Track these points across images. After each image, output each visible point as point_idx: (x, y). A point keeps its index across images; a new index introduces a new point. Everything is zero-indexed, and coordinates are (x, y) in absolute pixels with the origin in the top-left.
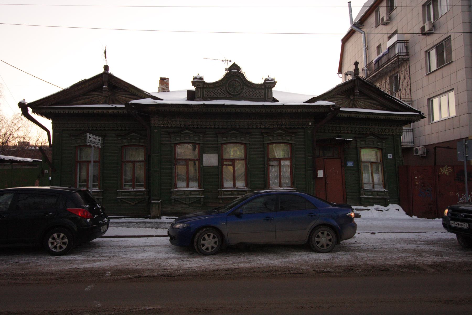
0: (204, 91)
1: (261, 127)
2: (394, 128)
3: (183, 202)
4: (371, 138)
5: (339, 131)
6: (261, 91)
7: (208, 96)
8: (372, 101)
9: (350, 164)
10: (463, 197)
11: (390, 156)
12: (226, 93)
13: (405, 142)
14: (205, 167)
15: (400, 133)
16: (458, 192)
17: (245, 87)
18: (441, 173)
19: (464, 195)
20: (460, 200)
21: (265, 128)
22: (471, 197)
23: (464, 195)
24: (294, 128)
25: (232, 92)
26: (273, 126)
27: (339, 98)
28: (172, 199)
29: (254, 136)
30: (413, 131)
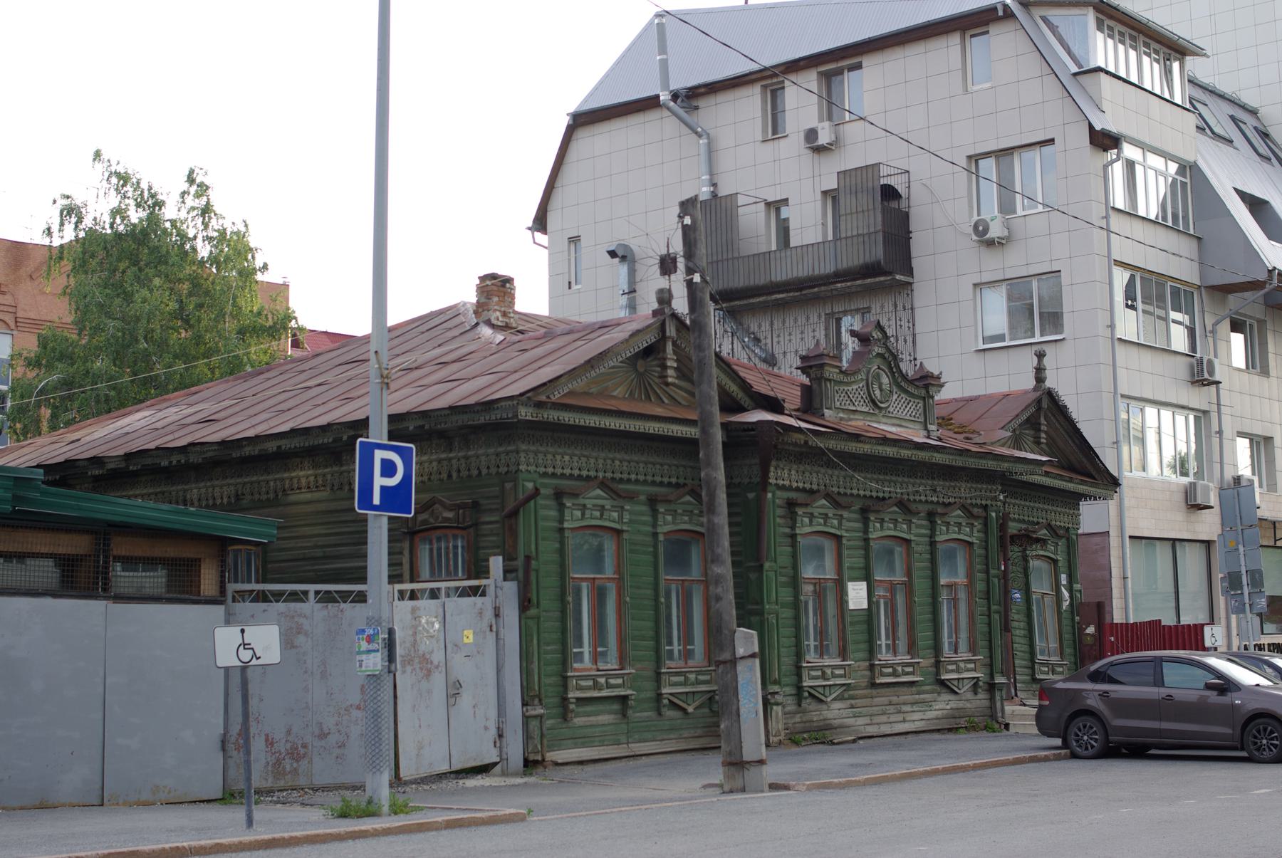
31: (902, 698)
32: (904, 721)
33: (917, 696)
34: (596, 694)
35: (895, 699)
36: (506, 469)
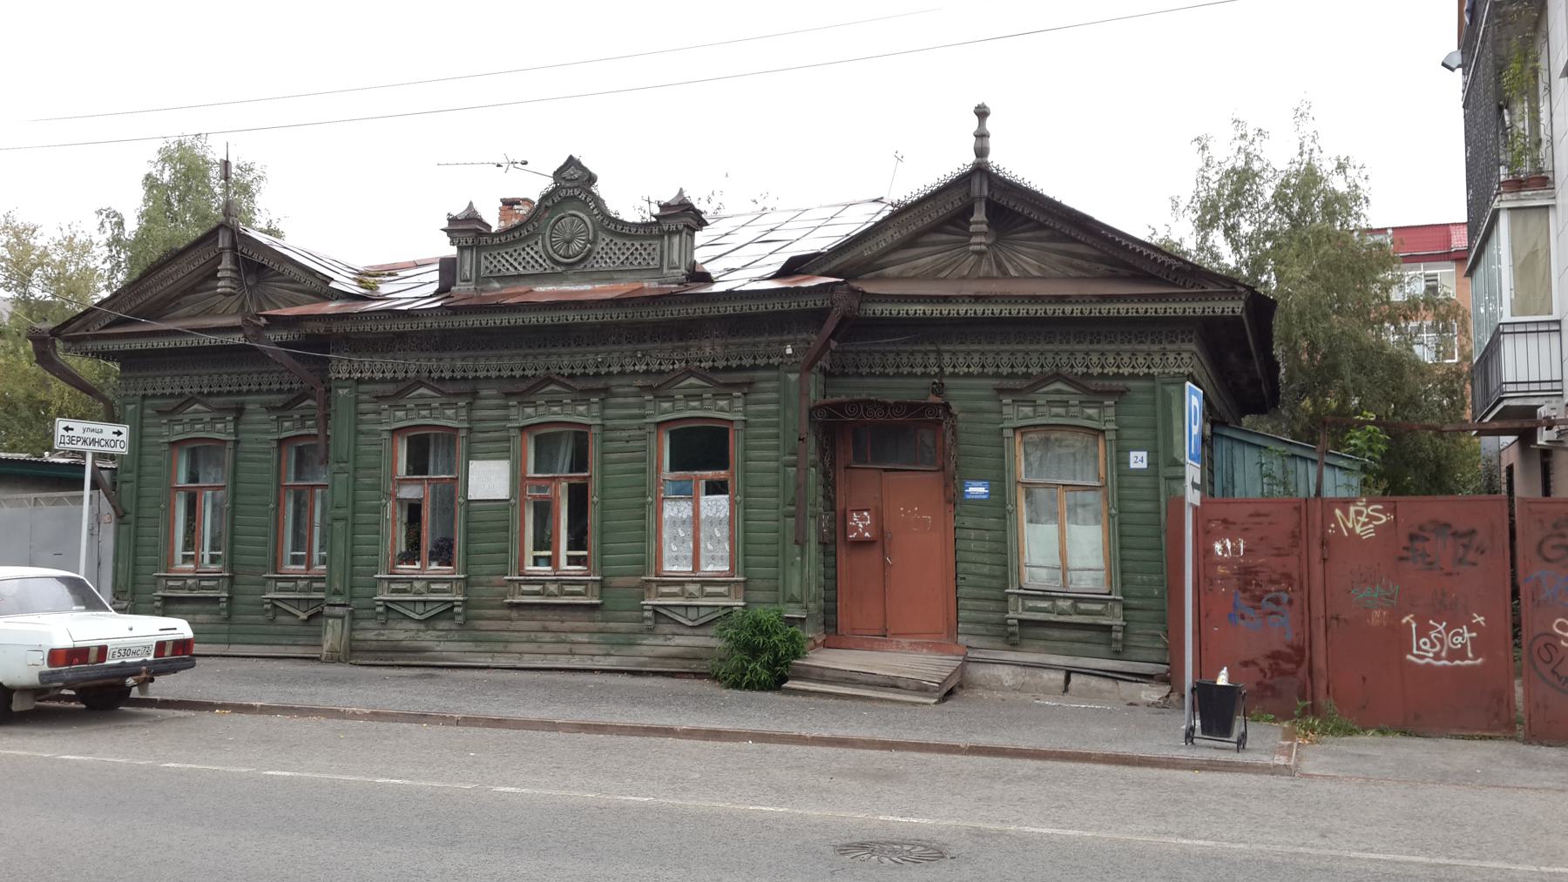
0: (483, 258)
1: (637, 368)
2: (1156, 347)
3: (407, 612)
4: (1058, 392)
5: (937, 370)
6: (650, 245)
7: (491, 272)
8: (1061, 246)
9: (977, 490)
10: (1433, 634)
11: (1139, 458)
12: (545, 261)
13: (1551, 381)
14: (472, 504)
15: (1179, 366)
16: (1410, 613)
17: (601, 235)
18: (1338, 527)
19: (1441, 625)
20: (1418, 643)
21: (647, 372)
22: (1474, 634)
23: (1441, 625)
24: (741, 368)
25: (560, 256)
26: (674, 364)
27: (943, 243)
28: (645, 607)
29: (621, 400)
30: (1559, 331)
31: (567, 625)
32: (572, 653)
33: (604, 624)
34: (1052, 617)
35: (555, 625)
36: (257, 387)
